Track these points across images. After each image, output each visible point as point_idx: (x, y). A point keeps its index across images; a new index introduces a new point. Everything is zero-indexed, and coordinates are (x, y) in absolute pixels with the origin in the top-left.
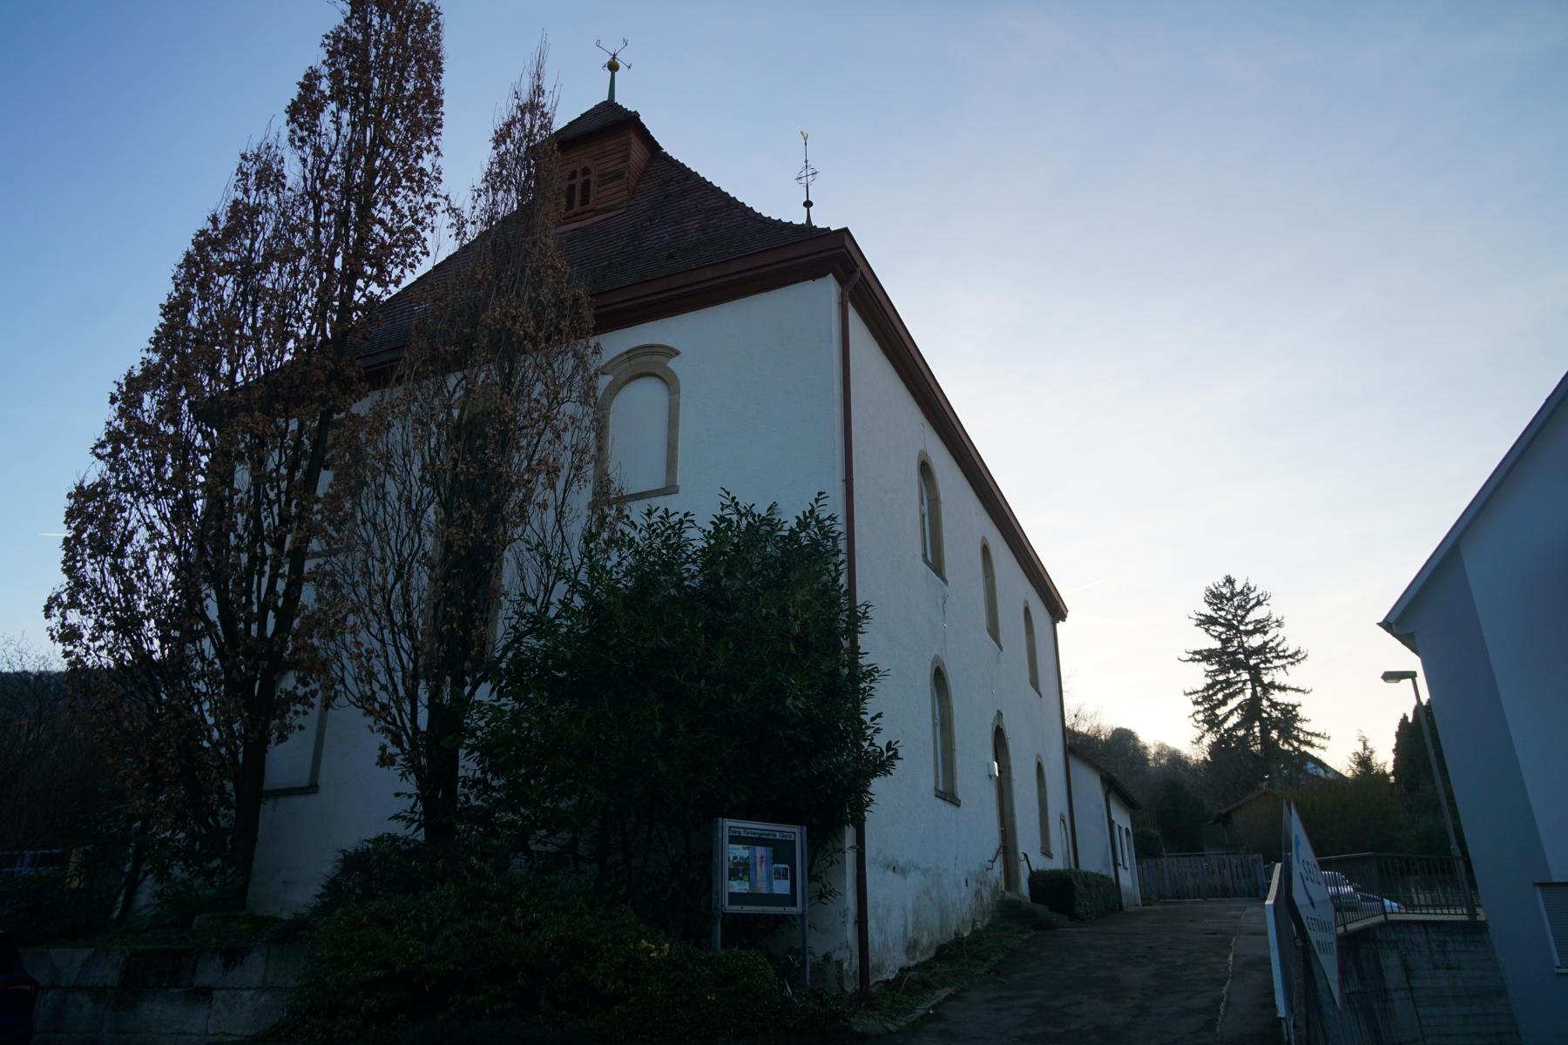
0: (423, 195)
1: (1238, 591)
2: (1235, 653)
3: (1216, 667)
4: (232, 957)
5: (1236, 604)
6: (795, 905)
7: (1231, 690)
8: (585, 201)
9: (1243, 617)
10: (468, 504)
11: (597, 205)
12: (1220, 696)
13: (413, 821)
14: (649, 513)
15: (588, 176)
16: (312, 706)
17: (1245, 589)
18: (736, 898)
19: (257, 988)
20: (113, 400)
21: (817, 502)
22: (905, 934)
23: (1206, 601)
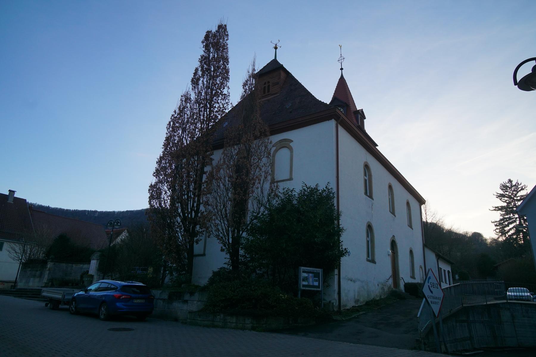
0: (225, 100)
1: (514, 185)
2: (512, 208)
3: (504, 213)
4: (192, 294)
5: (513, 189)
6: (319, 288)
7: (511, 221)
8: (268, 91)
9: (516, 194)
10: (239, 189)
12: (506, 223)
13: (229, 265)
14: (284, 189)
16: (203, 234)
17: (517, 184)
18: (304, 286)
19: (197, 301)
20: (157, 163)
21: (327, 184)
22: (355, 297)
23: (500, 189)
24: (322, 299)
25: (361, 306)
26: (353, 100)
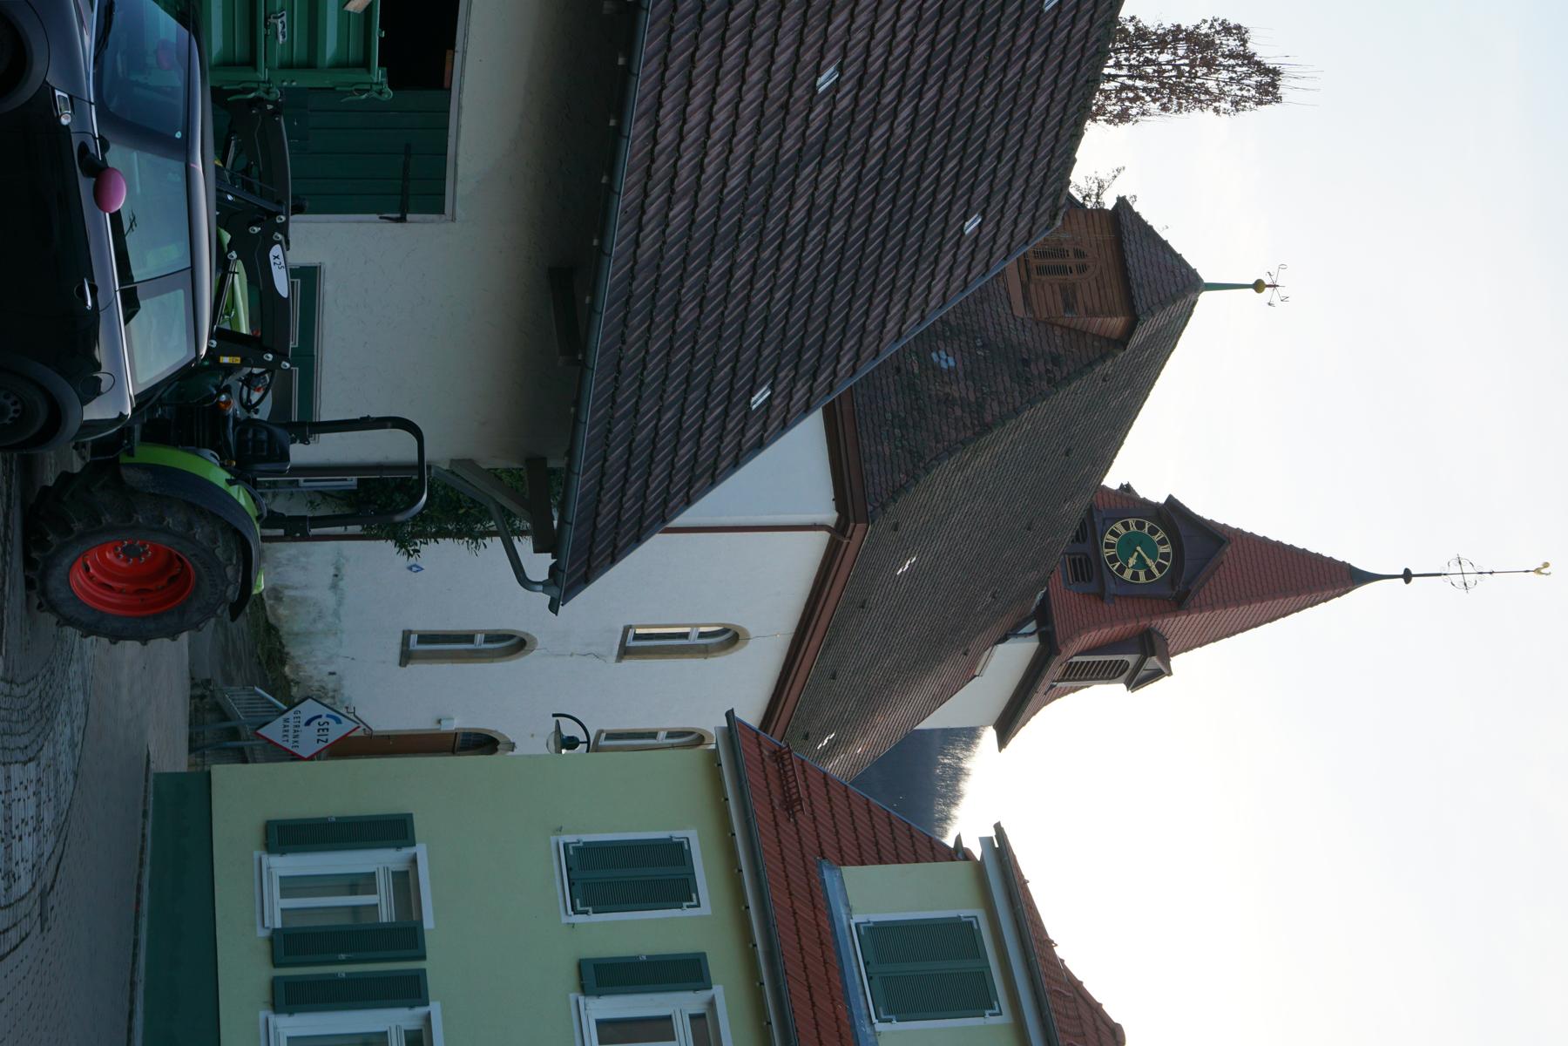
11: (1036, 284)
15: (1075, 271)
22: (287, 587)
24: (277, 490)
25: (264, 608)
26: (1234, 634)
